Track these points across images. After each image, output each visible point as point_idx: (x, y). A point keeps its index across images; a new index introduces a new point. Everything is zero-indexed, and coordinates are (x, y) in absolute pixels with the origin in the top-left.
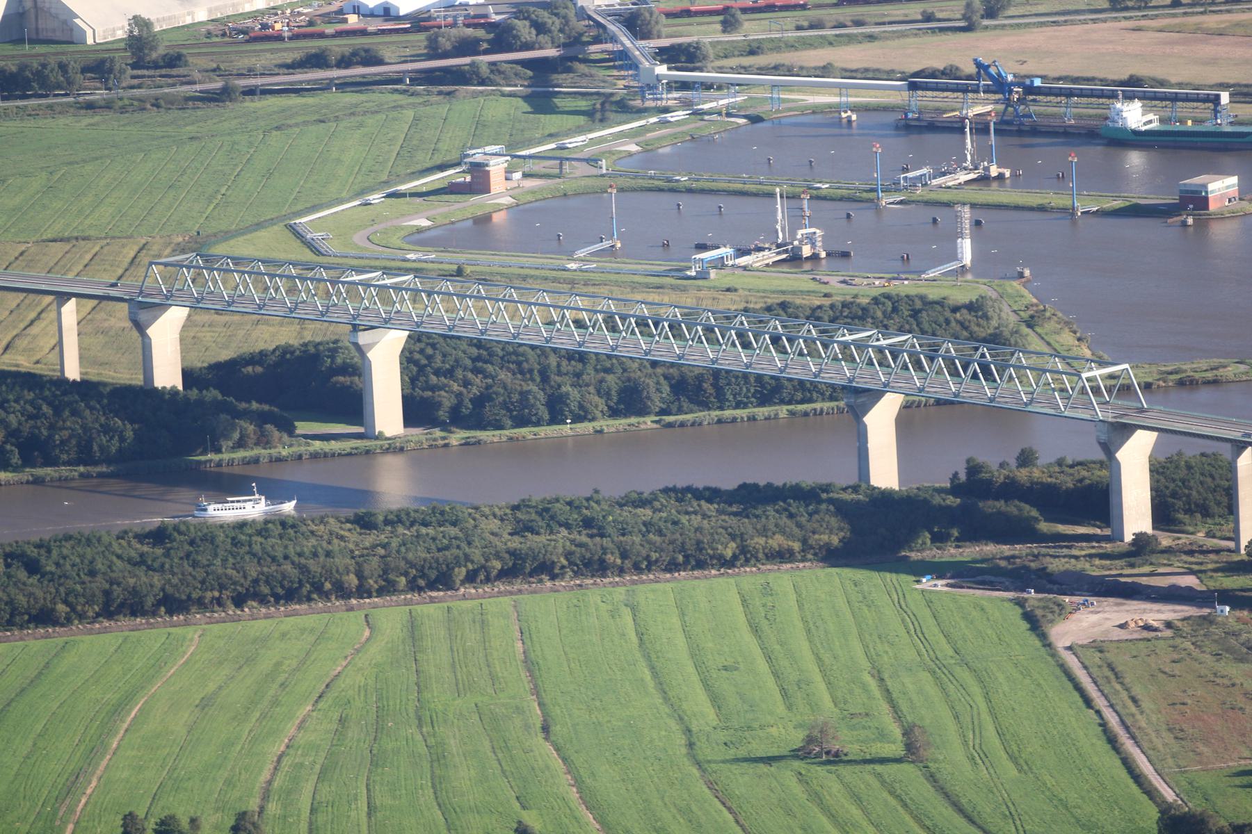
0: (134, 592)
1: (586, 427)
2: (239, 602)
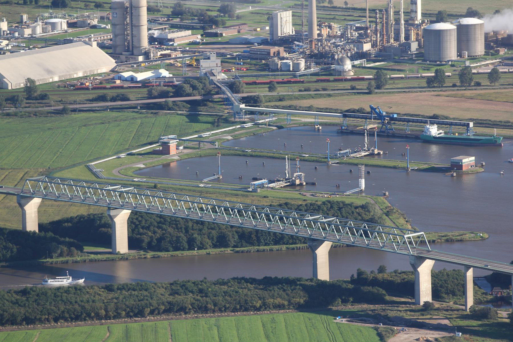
1: (203, 252)
2: (56, 320)
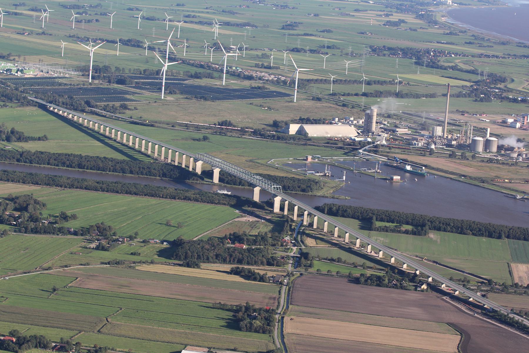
1: (243, 187)
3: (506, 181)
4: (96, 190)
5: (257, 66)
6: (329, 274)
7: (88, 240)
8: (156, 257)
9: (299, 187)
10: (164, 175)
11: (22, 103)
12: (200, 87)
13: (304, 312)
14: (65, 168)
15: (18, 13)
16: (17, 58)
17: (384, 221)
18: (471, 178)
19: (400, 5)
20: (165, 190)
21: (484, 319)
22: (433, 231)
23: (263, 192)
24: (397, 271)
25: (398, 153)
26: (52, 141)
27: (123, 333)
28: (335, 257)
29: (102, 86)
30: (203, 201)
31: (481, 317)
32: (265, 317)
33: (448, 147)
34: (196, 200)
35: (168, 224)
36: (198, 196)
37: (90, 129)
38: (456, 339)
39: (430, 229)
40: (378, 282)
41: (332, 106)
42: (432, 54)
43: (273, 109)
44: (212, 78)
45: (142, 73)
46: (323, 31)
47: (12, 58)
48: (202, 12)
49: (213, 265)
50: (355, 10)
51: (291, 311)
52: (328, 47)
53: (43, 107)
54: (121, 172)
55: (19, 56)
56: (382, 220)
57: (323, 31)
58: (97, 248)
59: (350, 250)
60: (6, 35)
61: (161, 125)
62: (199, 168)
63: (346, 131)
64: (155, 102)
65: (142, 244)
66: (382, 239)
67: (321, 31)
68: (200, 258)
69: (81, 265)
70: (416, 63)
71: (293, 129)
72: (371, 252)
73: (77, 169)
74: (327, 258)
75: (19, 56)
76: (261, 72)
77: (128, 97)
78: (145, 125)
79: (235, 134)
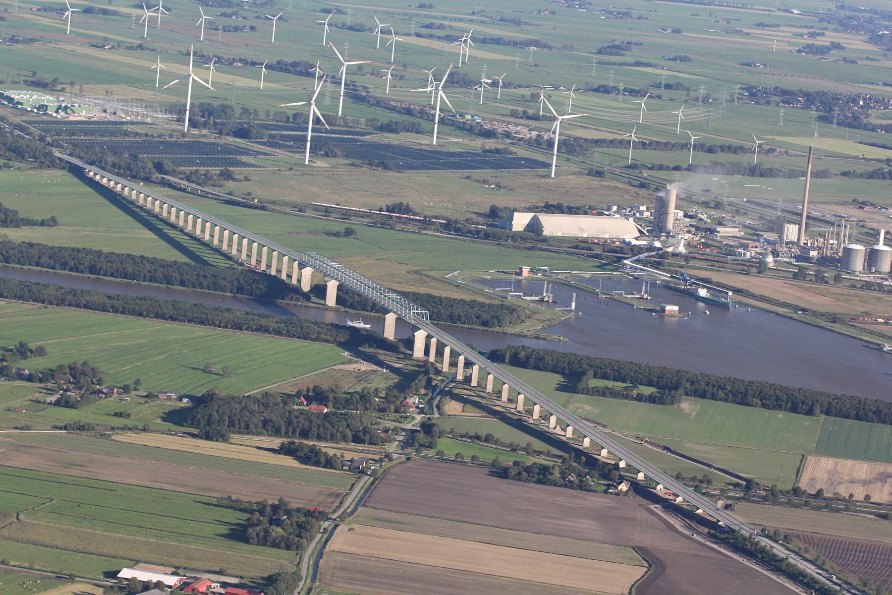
0: (164, 313)
1: (377, 315)
2: (189, 322)
3: (880, 320)
4: (103, 309)
5: (514, 114)
6: (458, 460)
7: (48, 389)
8: (159, 421)
9: (478, 318)
10: (240, 290)
11: (42, 162)
12: (389, 147)
13: (379, 520)
14: (67, 272)
15: (110, 11)
16: (68, 87)
17: (608, 379)
18: (815, 314)
19: (849, 18)
20: (226, 314)
21: (708, 543)
22: (692, 398)
23: (400, 321)
24: (584, 459)
25: (700, 268)
26: (67, 228)
27: (35, 538)
28: (483, 433)
29: (204, 140)
30: (290, 335)
31: (702, 541)
32: (297, 522)
33: (802, 261)
34: (279, 333)
35: (207, 370)
36: (282, 325)
37: (146, 211)
38: (637, 572)
39: (687, 394)
40: (541, 476)
41: (620, 185)
42: (861, 103)
43: (505, 188)
44: (418, 132)
45: (291, 120)
46: (675, 59)
47: (60, 87)
48: (461, 20)
49: (254, 437)
50: (758, 25)
51: (357, 516)
52: (668, 87)
53: (78, 172)
54: (164, 281)
55: (72, 84)
56: (605, 377)
57: (675, 59)
58: (57, 403)
59: (519, 424)
60: (69, 47)
61: (276, 207)
62: (307, 279)
63: (620, 228)
64: (291, 169)
65: (143, 400)
66: (589, 408)
67: (670, 59)
68: (234, 426)
69: (17, 428)
70: (821, 118)
71: (521, 220)
72: (555, 428)
73: (87, 275)
74: (467, 433)
75: (72, 84)
76: (517, 125)
77: (244, 159)
78: (250, 207)
79: (411, 226)
